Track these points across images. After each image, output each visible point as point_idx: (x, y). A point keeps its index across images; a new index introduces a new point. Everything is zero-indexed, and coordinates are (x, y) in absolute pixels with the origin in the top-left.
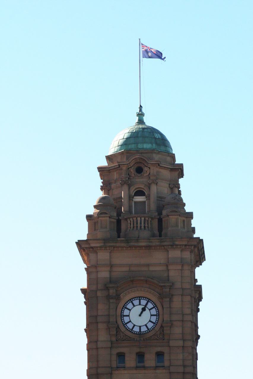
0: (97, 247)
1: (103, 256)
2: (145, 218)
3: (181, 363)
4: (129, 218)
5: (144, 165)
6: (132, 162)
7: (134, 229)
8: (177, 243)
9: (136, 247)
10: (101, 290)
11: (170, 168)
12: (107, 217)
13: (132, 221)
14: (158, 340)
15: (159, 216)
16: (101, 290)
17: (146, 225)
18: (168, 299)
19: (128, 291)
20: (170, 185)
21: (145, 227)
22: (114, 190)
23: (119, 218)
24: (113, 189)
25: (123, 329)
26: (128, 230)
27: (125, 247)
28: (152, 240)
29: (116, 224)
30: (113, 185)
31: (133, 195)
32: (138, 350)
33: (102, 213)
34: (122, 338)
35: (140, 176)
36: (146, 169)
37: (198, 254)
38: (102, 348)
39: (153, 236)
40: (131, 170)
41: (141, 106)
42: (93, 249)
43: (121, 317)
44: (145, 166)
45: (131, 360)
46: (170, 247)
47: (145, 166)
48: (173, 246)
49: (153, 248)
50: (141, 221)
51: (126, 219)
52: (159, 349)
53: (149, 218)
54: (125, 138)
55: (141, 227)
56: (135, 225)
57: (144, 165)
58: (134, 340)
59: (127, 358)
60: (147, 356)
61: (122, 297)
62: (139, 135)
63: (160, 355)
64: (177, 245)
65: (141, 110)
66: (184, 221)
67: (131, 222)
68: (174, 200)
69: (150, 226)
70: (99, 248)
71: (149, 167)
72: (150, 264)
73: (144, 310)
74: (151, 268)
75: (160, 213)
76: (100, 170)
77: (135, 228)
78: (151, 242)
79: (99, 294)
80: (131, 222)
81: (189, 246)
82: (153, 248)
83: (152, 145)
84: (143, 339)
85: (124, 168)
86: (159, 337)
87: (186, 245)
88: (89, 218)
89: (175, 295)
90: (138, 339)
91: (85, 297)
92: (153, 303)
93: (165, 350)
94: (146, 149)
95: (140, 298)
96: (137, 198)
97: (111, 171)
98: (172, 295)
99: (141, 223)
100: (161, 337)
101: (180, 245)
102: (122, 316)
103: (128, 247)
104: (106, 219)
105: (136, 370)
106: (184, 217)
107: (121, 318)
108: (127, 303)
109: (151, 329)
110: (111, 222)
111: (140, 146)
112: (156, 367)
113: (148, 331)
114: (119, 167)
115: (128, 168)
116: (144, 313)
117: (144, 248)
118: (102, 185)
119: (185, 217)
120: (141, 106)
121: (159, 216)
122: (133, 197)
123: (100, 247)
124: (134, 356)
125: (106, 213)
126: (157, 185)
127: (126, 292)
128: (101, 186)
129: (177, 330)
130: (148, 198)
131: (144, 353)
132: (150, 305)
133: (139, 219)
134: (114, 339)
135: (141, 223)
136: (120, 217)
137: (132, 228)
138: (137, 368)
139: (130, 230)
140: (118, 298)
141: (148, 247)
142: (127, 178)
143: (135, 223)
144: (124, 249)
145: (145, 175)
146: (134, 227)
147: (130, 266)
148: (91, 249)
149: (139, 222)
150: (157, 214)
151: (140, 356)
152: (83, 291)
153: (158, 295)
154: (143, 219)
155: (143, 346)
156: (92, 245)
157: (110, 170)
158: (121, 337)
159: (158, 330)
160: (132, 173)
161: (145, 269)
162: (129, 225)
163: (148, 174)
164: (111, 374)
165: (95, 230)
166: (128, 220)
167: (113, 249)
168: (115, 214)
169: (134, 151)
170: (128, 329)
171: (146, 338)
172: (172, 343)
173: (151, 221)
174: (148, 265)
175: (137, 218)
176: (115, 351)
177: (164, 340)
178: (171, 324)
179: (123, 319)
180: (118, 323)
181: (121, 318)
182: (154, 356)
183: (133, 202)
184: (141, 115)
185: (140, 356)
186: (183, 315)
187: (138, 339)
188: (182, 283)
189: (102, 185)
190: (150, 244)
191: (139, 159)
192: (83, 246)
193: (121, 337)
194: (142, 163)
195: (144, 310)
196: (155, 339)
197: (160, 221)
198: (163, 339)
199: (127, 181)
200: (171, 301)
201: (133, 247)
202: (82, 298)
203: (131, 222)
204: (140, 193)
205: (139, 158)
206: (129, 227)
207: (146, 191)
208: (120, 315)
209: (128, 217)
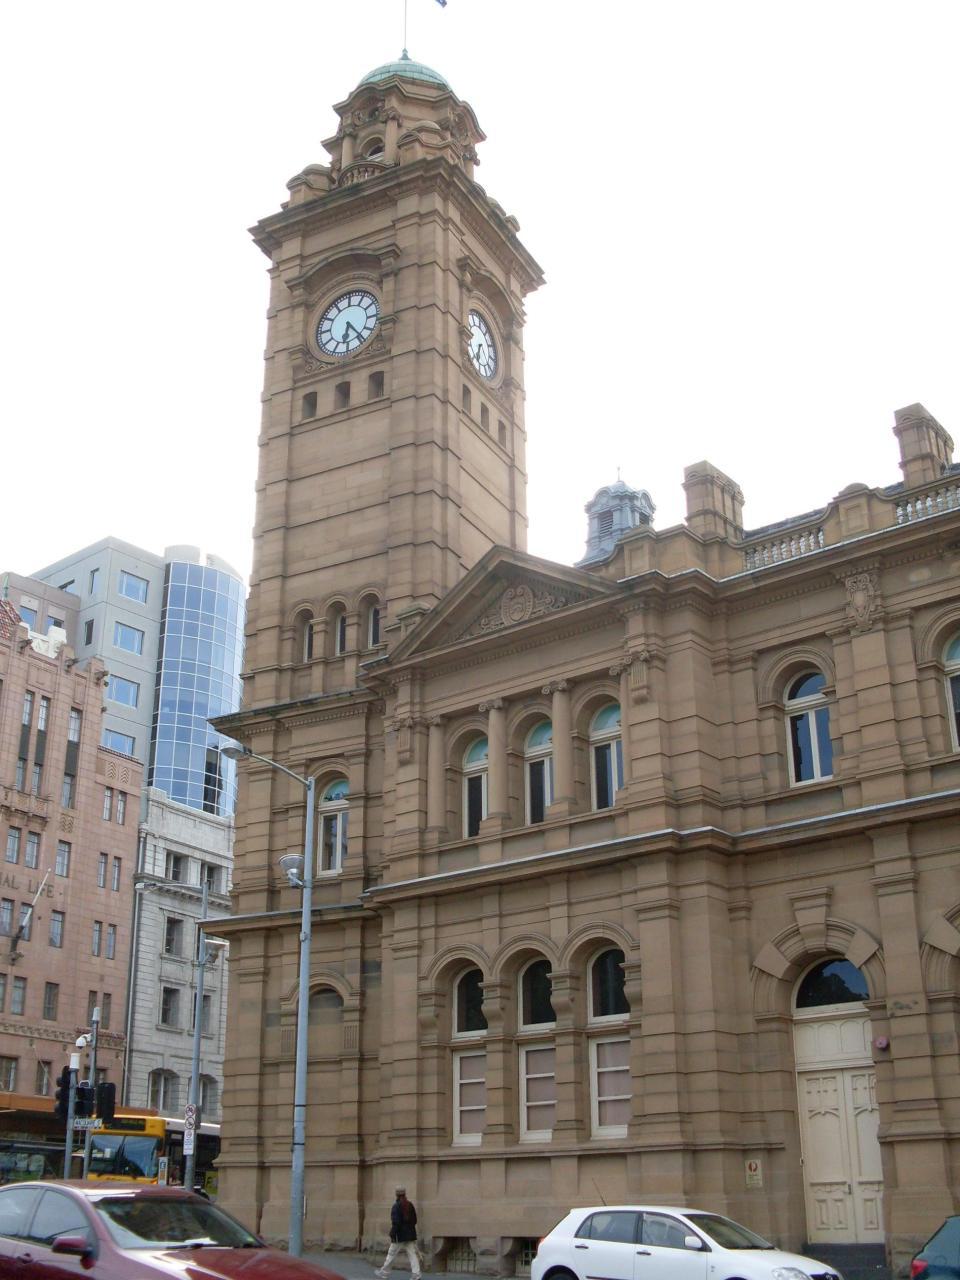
45: (327, 402)
185: (344, 390)
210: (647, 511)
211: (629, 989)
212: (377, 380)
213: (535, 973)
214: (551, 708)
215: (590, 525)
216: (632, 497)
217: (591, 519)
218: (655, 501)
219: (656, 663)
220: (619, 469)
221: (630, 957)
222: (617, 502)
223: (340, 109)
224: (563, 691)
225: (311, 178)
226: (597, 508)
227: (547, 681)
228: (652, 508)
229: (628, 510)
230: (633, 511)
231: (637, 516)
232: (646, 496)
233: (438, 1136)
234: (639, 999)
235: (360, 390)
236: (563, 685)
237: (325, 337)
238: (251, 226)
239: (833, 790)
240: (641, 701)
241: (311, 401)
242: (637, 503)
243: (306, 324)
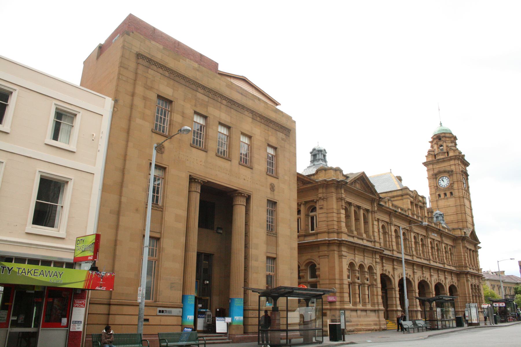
45: (442, 196)
63: (451, 193)
151: (445, 194)
176: (437, 194)
184: (441, 122)
185: (445, 194)
210: (325, 154)
211: (317, 273)
212: (451, 193)
213: (361, 266)
214: (301, 207)
215: (311, 158)
216: (321, 151)
217: (312, 155)
218: (327, 151)
219: (325, 200)
220: (391, 170)
221: (318, 266)
222: (318, 152)
223: (464, 156)
224: (304, 204)
225: (430, 152)
226: (313, 154)
227: (301, 201)
228: (326, 153)
229: (320, 154)
230: (322, 154)
231: (323, 155)
232: (325, 150)
233: (140, 287)
234: (319, 276)
235: (448, 194)
236: (304, 203)
237: (441, 186)
238: (424, 162)
239: (317, 234)
240: (321, 208)
241: (439, 195)
242: (322, 152)
243: (436, 181)
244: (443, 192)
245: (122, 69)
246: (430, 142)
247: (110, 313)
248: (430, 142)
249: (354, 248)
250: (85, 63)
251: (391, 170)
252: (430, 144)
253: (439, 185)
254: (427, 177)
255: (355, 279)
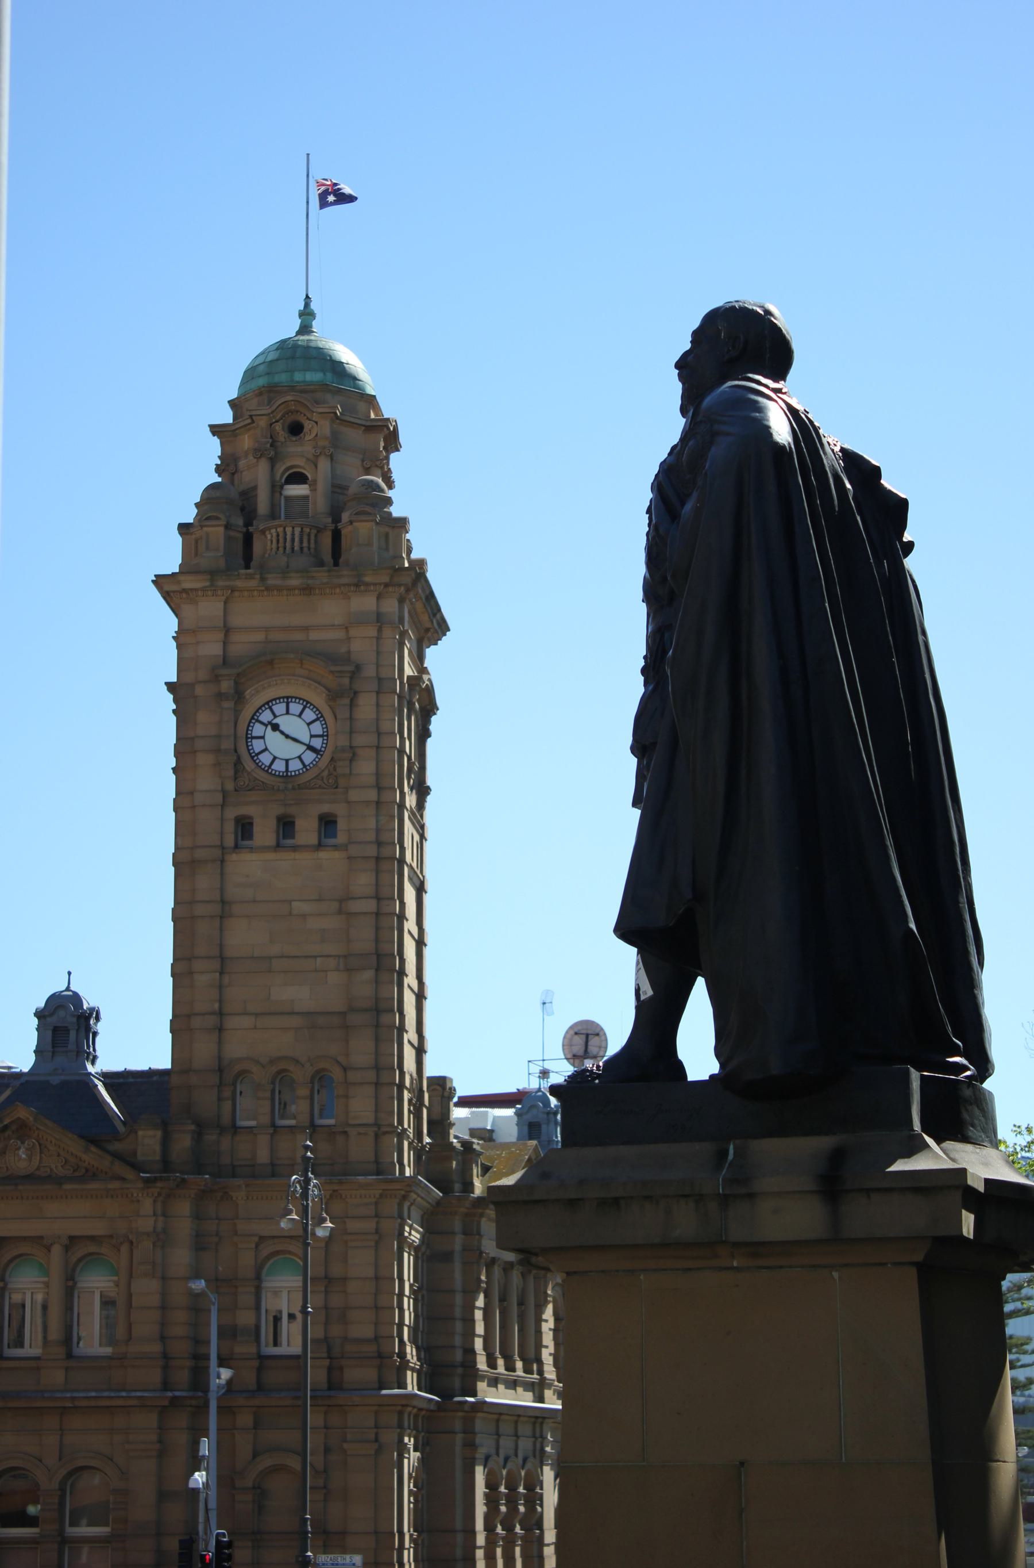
0: (196, 590)
1: (211, 608)
2: (302, 529)
3: (371, 836)
4: (269, 529)
5: (306, 417)
6: (279, 408)
7: (278, 552)
8: (367, 579)
9: (279, 589)
10: (205, 682)
11: (364, 426)
12: (218, 526)
13: (275, 534)
14: (324, 788)
15: (334, 525)
16: (205, 682)
17: (305, 544)
18: (347, 701)
19: (260, 684)
20: (363, 461)
21: (302, 548)
22: (244, 473)
23: (248, 530)
24: (242, 472)
25: (249, 765)
26: (267, 555)
27: (248, 591)
28: (315, 574)
29: (241, 542)
30: (242, 463)
31: (283, 480)
32: (280, 811)
33: (209, 517)
34: (246, 784)
35: (296, 441)
36: (307, 425)
37: (425, 610)
38: (204, 805)
39: (321, 564)
40: (277, 428)
41: (307, 297)
42: (189, 594)
43: (247, 740)
44: (308, 418)
45: (265, 832)
46: (352, 588)
47: (308, 418)
48: (358, 585)
49: (317, 591)
50: (293, 534)
51: (263, 532)
52: (326, 808)
53: (310, 530)
54: (269, 360)
55: (293, 549)
56: (281, 544)
57: (306, 417)
58: (273, 788)
59: (256, 829)
60: (300, 824)
61: (248, 697)
62: (298, 354)
63: (328, 823)
64: (367, 584)
65: (307, 305)
66: (387, 535)
67: (272, 536)
68: (366, 489)
69: (312, 546)
70: (200, 593)
71: (316, 420)
72: (311, 626)
73: (276, 727)
74: (314, 636)
75: (337, 520)
76: (215, 430)
77: (281, 549)
78: (313, 577)
79: (199, 690)
80: (272, 536)
81: (394, 585)
82: (317, 591)
83: (324, 374)
84: (293, 786)
85: (263, 423)
86: (325, 781)
87: (386, 585)
88: (184, 529)
89: (362, 692)
90: (282, 786)
91: (175, 701)
92: (316, 709)
93: (339, 809)
94: (310, 384)
95: (288, 699)
96: (294, 489)
97: (237, 431)
98: (356, 693)
99: (293, 540)
100: (330, 781)
101: (375, 584)
102: (325, 736)
103: (263, 590)
104: (217, 532)
105: (275, 851)
106: (387, 525)
107: (247, 742)
108: (259, 710)
109: (311, 765)
110: (228, 539)
111: (298, 377)
112: (320, 846)
113: (304, 770)
114: (253, 422)
115: (269, 423)
116: (282, 728)
117: (297, 592)
118: (219, 463)
119: (390, 526)
120: (307, 297)
121: (334, 525)
122: (282, 487)
123: (204, 589)
124: (273, 823)
125: (217, 518)
126: (332, 459)
127: (256, 686)
128: (217, 465)
129: (365, 768)
130: (313, 490)
131: (294, 817)
132: (266, 716)
133: (289, 530)
134: (230, 786)
135: (293, 540)
136: (250, 528)
137: (274, 549)
138: (278, 846)
139: (269, 554)
140: (239, 697)
141: (307, 590)
142: (269, 445)
143: (281, 540)
144: (265, 594)
145: (308, 438)
146: (278, 548)
147: (267, 629)
148: (184, 595)
149: (289, 537)
150: (330, 520)
151: (286, 826)
152: (171, 687)
153: (327, 692)
154: (297, 530)
155: (292, 802)
156: (187, 585)
157: (236, 429)
158: (244, 783)
159: (325, 768)
160: (280, 434)
161: (299, 636)
162: (269, 543)
163: (313, 435)
164: (223, 861)
165: (196, 554)
166: (267, 532)
167: (231, 593)
168: (240, 522)
169: (286, 388)
170: (260, 767)
171: (299, 785)
172: (354, 795)
173: (316, 536)
174: (307, 629)
175: (285, 529)
176: (231, 813)
177: (337, 787)
178: (353, 753)
179: (252, 745)
180: (238, 751)
181: (247, 742)
182: (315, 824)
183: (282, 497)
184: (307, 314)
185: (286, 826)
186: (379, 734)
187: (282, 786)
188: (378, 666)
189: (219, 463)
190: (310, 582)
191: (293, 403)
192: (167, 588)
193: (244, 783)
194: (301, 413)
195: (276, 727)
196: (317, 786)
197: (337, 536)
198: (336, 785)
199: (266, 450)
200: (352, 705)
201: (273, 590)
202: (168, 702)
203: (273, 538)
204: (298, 478)
205: (292, 401)
206: (268, 547)
207: (305, 469)
208: (245, 736)
209: (267, 526)
212: (328, 823)
220: (69, 973)
241: (245, 827)
244: (277, 810)
245: (256, 1239)
246: (216, 430)
247: (269, 1162)
248: (216, 430)
249: (515, 1418)
250: (35, 1052)
251: (69, 973)
252: (214, 447)
253: (254, 757)
254: (234, 395)
255: (552, 1294)
